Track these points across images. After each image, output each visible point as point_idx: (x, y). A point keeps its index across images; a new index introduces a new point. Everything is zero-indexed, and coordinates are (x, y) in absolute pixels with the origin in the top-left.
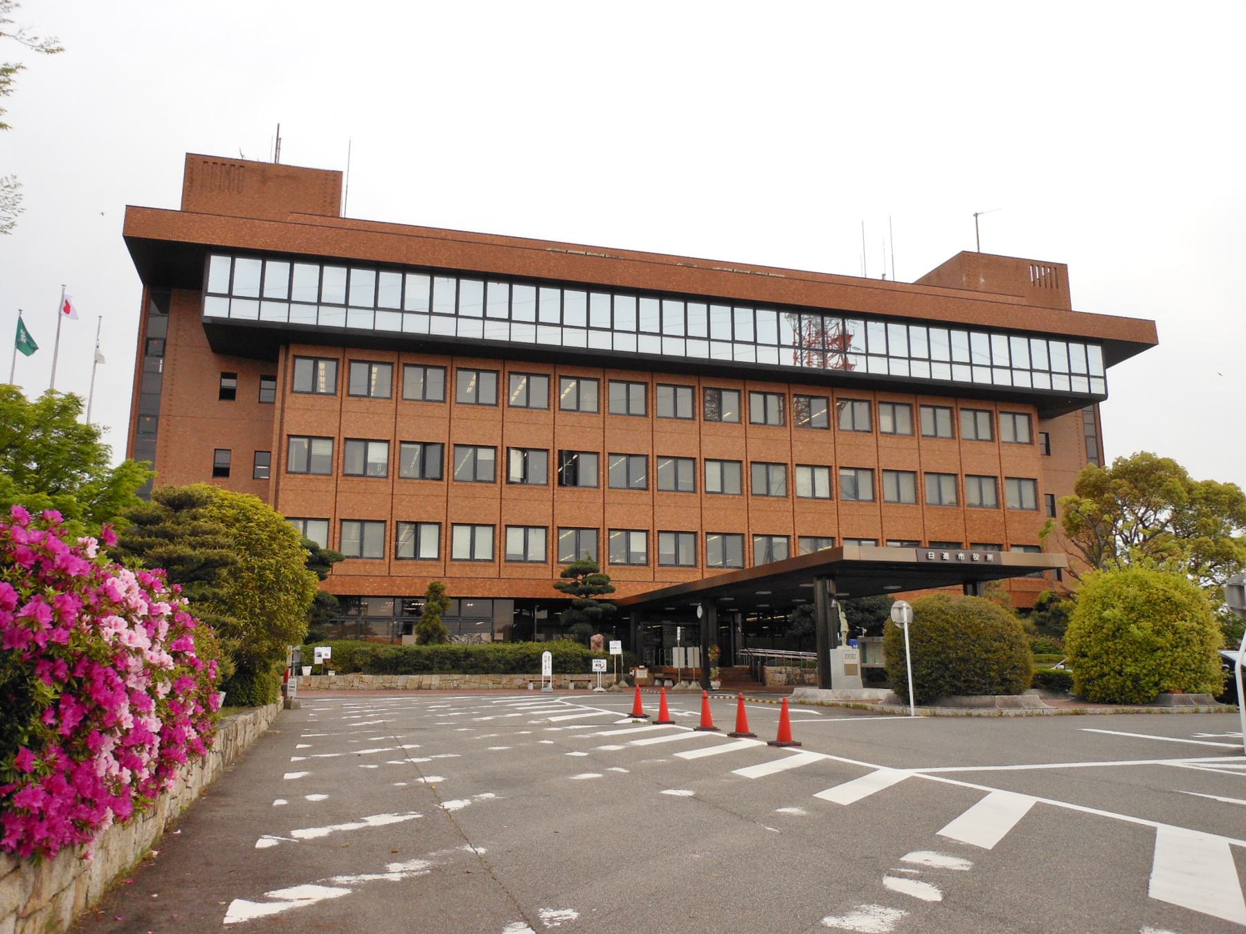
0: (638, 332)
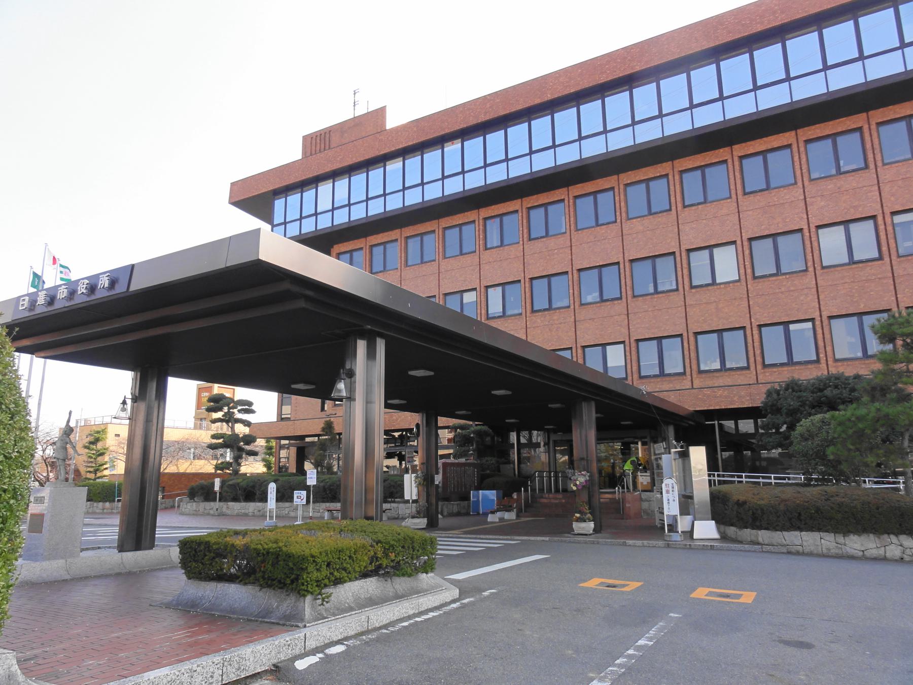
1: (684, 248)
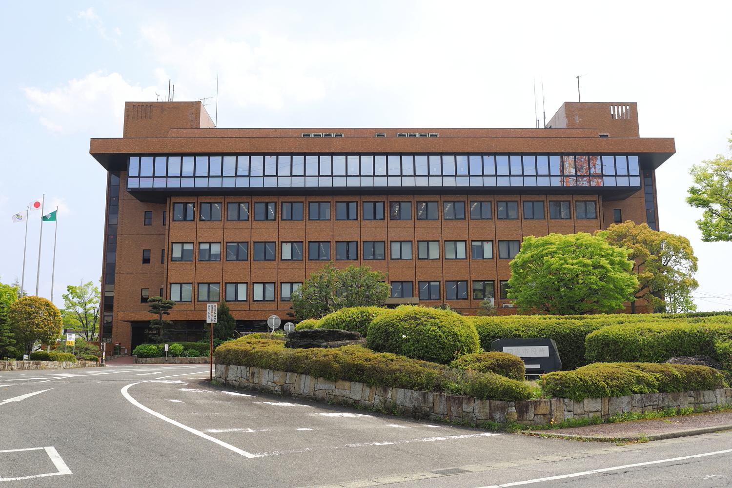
0: (616, 175)
1: (389, 239)
